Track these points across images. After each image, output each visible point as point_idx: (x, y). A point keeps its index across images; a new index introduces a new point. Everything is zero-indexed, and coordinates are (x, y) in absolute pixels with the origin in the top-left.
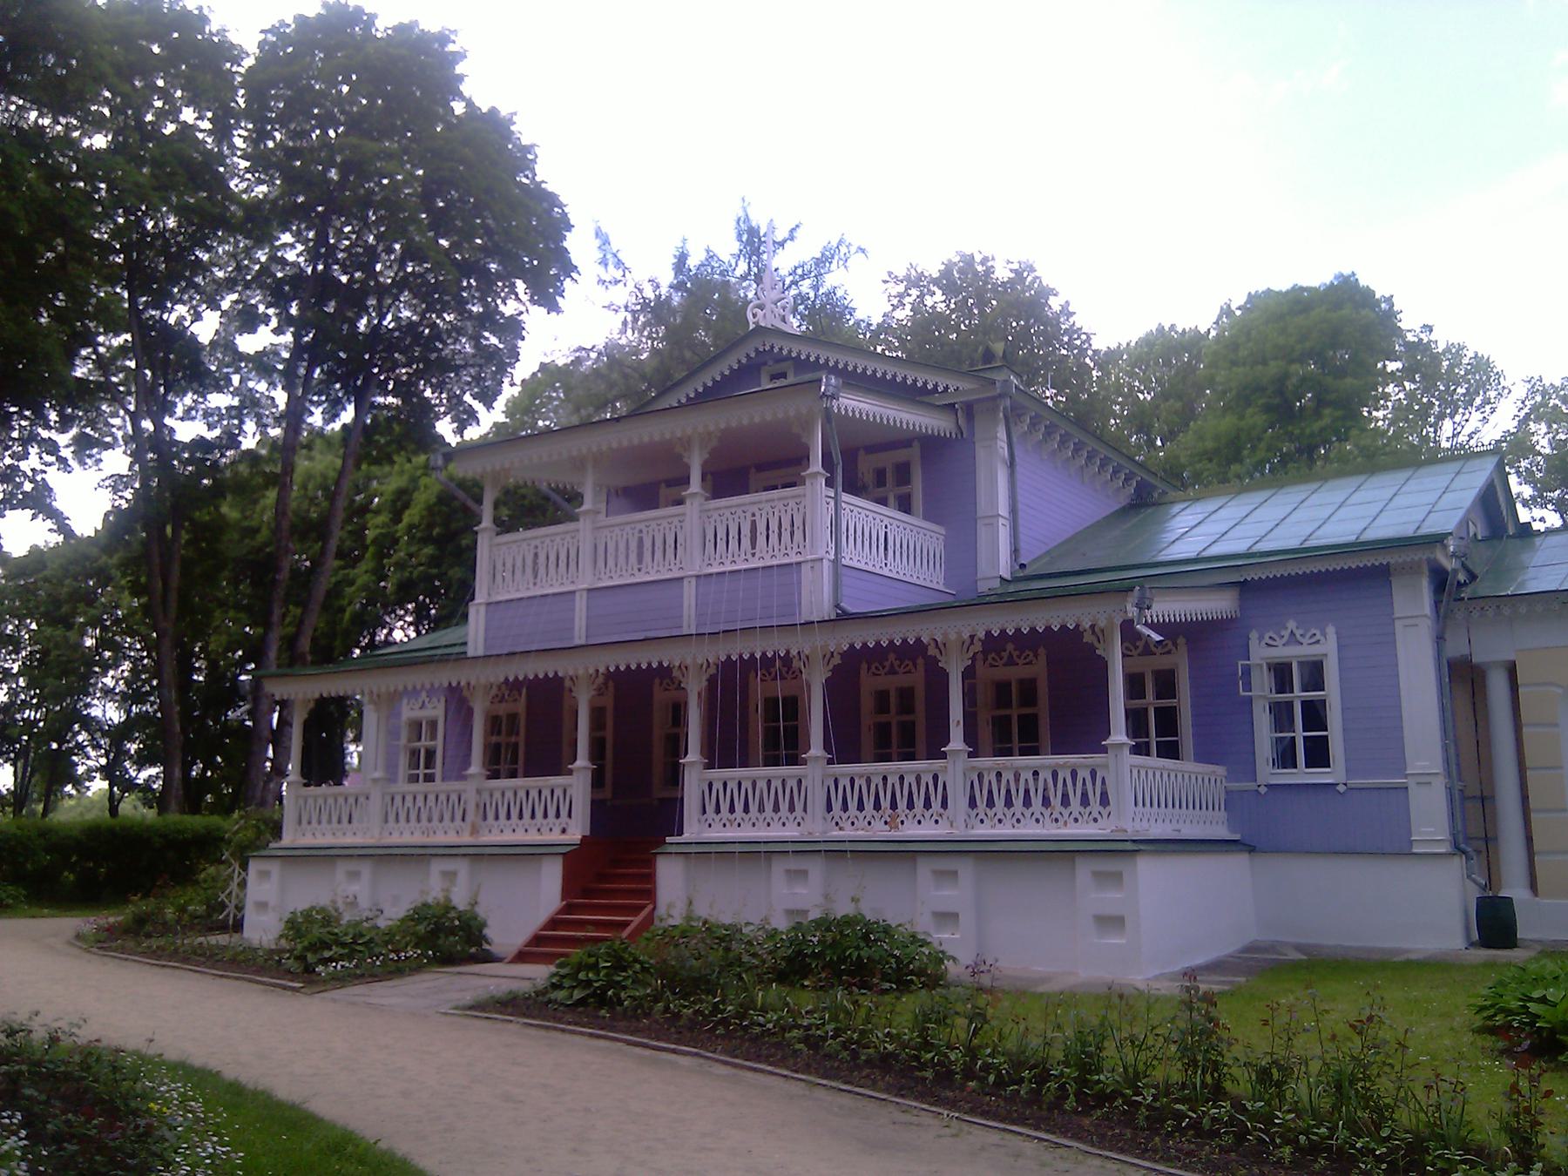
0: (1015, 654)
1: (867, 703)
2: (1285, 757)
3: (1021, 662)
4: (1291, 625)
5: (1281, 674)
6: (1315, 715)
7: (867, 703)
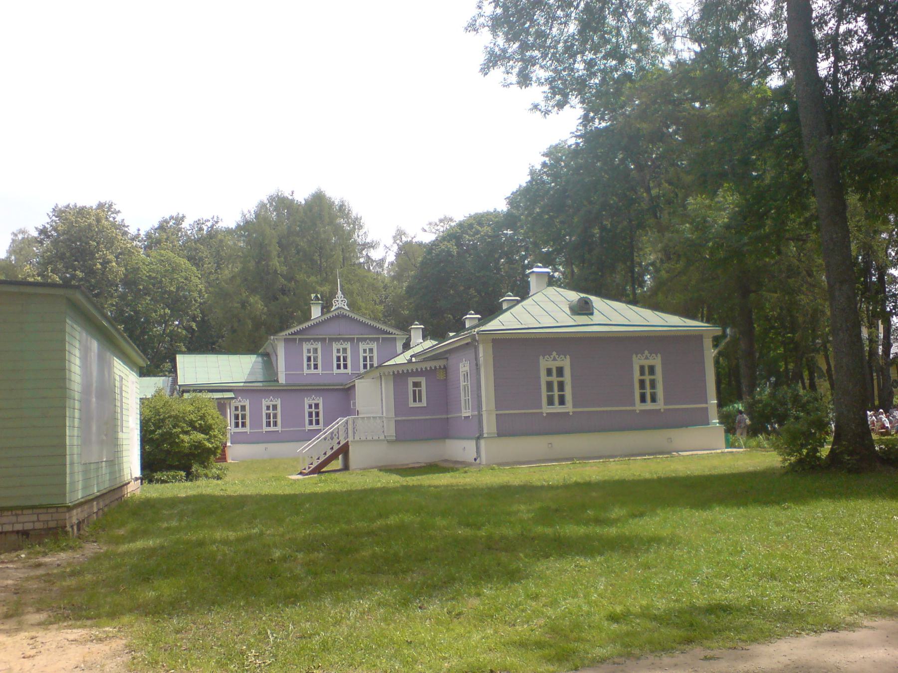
2: (268, 424)
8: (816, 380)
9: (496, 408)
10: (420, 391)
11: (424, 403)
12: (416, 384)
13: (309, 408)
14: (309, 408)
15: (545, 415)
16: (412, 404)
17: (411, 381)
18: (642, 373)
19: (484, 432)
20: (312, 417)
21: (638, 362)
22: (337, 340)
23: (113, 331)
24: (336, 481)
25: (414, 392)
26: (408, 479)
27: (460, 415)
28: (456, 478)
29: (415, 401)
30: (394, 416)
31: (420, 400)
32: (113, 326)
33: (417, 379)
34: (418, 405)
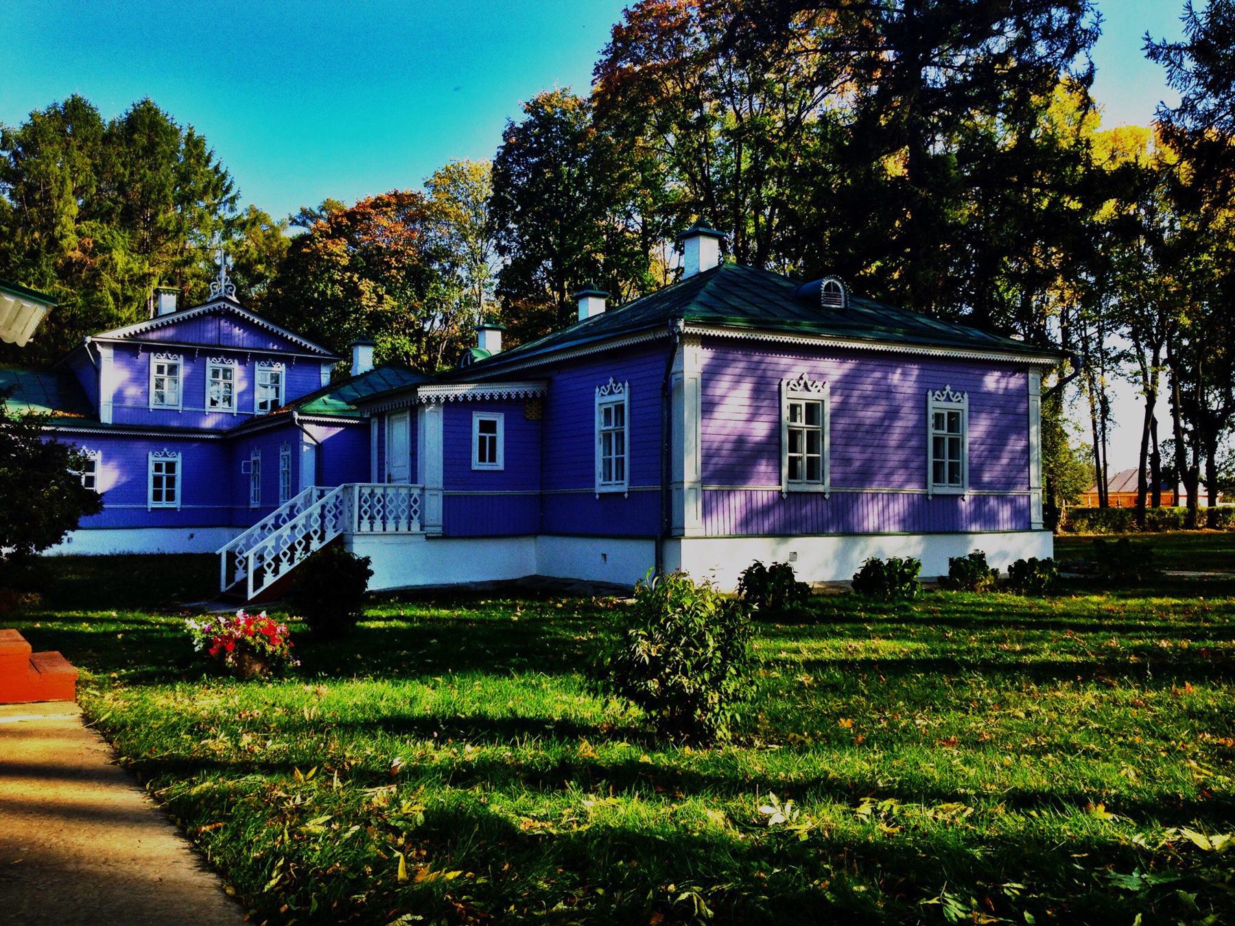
0: (951, 393)
1: (151, 467)
2: (157, 496)
3: (954, 399)
4: (165, 450)
5: (158, 467)
6: (171, 482)
7: (151, 467)
8: (1093, 444)
9: (444, 484)
10: (493, 440)
11: (500, 464)
12: (488, 427)
13: (156, 471)
14: (156, 471)
15: (597, 497)
16: (476, 465)
17: (477, 417)
18: (938, 425)
19: (1185, 499)
20: (161, 486)
21: (477, 417)
22: (215, 354)
23: (211, 307)
24: (836, 649)
25: (482, 440)
26: (410, 688)
27: (588, 490)
28: (867, 650)
29: (482, 459)
30: (441, 486)
31: (493, 459)
32: (207, 303)
33: (488, 417)
34: (487, 466)
